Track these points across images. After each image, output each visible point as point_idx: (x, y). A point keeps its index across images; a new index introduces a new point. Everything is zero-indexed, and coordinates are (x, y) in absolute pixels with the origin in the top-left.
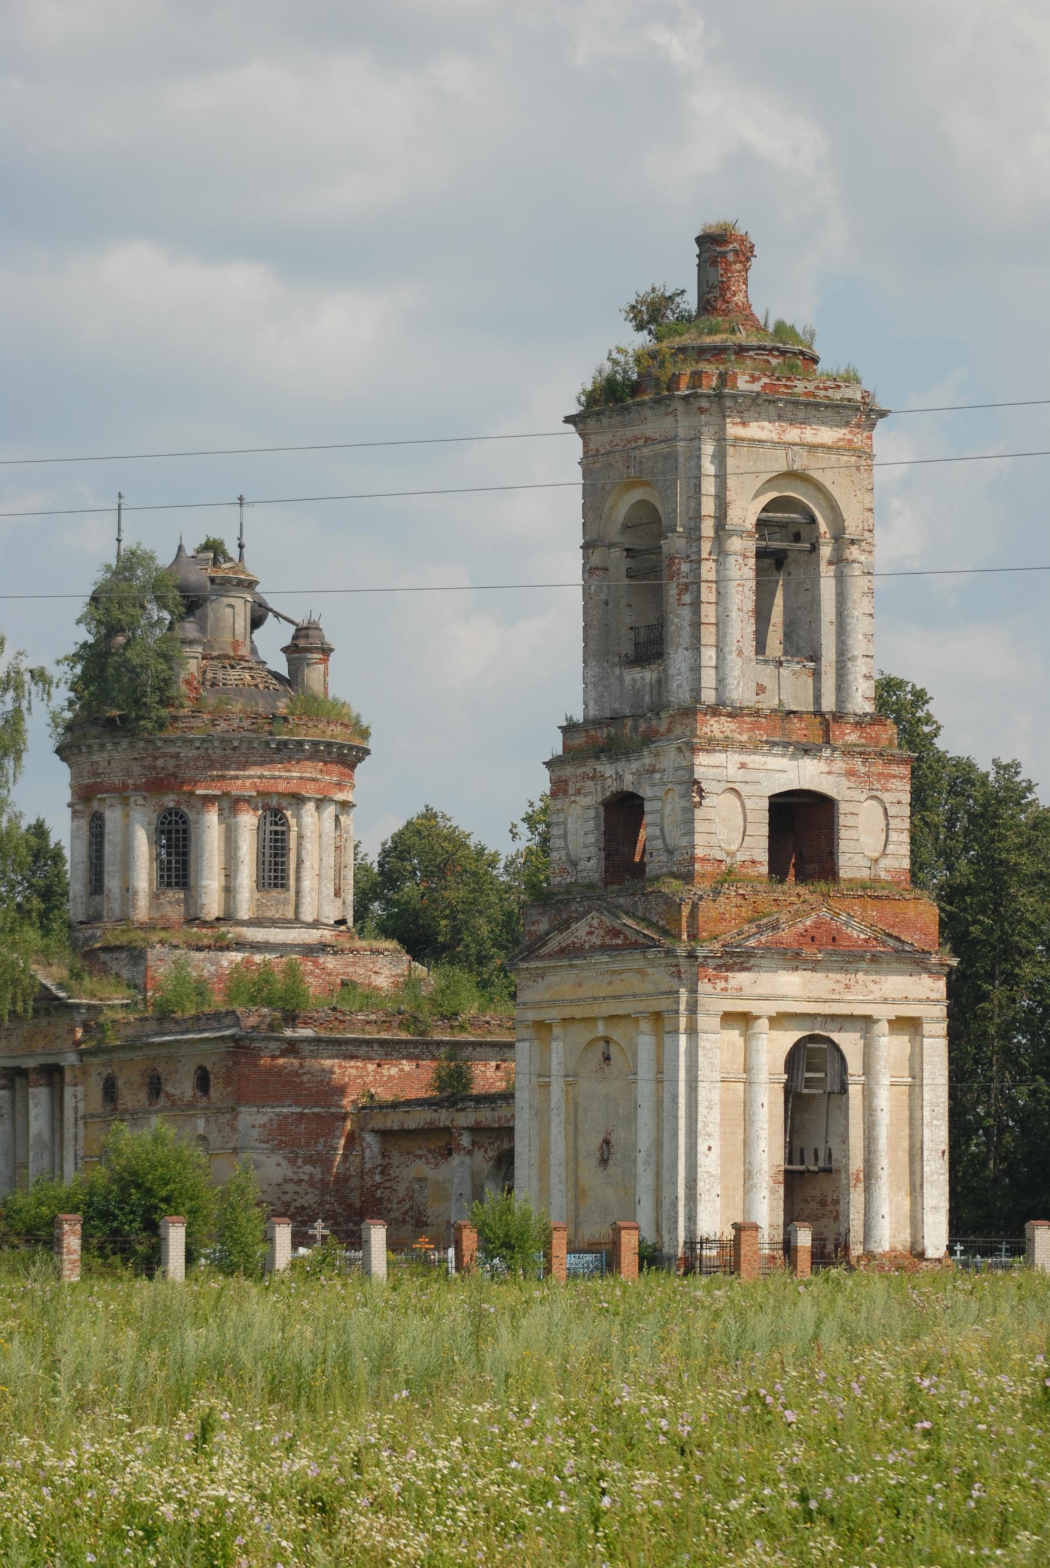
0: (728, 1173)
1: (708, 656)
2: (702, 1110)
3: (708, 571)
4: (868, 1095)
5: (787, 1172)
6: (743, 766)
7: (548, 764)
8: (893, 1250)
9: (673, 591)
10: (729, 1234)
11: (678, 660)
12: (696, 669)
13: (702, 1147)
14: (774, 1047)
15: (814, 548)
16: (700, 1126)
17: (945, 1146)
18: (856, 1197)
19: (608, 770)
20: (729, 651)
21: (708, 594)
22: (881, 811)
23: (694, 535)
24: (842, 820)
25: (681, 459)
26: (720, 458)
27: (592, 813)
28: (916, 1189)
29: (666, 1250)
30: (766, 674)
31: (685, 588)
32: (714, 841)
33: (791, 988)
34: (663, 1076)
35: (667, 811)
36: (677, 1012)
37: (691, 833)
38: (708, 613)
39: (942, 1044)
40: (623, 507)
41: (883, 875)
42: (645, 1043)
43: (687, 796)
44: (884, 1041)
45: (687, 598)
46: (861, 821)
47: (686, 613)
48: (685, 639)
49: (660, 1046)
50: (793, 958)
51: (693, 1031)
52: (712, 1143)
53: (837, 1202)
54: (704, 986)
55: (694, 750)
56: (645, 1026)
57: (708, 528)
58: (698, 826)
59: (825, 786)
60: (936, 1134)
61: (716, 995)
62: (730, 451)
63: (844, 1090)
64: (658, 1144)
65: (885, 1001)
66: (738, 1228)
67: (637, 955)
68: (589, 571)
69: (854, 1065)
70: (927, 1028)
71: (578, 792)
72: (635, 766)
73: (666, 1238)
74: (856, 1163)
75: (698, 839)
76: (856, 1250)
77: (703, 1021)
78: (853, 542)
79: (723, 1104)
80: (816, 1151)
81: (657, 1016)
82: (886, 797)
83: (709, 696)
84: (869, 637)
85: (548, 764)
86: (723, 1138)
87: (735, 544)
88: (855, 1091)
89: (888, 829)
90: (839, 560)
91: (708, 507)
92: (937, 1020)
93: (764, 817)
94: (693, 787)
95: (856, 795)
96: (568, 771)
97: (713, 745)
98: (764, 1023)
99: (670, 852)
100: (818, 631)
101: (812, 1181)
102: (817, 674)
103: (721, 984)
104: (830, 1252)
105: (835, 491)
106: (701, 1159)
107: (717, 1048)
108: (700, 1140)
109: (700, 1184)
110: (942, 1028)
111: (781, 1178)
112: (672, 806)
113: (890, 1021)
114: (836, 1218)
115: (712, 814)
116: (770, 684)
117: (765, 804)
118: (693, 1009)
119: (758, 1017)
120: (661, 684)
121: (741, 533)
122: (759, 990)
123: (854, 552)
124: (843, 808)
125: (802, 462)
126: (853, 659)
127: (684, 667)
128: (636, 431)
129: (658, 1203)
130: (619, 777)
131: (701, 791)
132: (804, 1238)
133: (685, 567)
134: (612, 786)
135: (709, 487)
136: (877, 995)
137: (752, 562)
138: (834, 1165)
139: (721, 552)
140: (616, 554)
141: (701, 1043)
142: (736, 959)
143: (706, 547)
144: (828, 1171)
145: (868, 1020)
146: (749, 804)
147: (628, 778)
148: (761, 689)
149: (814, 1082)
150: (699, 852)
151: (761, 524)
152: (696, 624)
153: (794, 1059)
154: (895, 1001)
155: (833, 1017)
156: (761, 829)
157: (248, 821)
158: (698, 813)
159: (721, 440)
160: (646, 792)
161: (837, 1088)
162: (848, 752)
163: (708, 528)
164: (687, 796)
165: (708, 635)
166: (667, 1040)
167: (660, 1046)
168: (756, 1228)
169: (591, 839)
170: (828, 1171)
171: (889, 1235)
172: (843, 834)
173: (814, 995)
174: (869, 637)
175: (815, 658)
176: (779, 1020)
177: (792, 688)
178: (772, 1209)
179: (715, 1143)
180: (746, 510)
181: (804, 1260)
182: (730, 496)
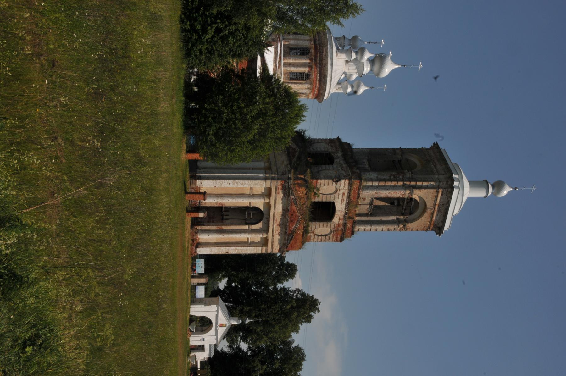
0: (218, 190)
1: (376, 184)
2: (242, 181)
3: (401, 183)
4: (245, 231)
5: (222, 207)
6: (343, 194)
7: (338, 138)
8: (199, 239)
9: (394, 173)
10: (202, 190)
11: (374, 175)
12: (372, 180)
13: (230, 181)
14: (259, 203)
15: (403, 214)
16: (237, 181)
17: (229, 253)
18: (214, 228)
19: (340, 154)
20: (373, 192)
21: (394, 183)
22: (327, 233)
23: (410, 180)
24: (325, 223)
25: (432, 176)
26: (432, 187)
27: (326, 150)
28: (218, 244)
29: (198, 170)
30: (368, 201)
31: (395, 177)
32: (322, 185)
33: (278, 209)
34: (253, 169)
35: (330, 171)
36: (272, 174)
37: (325, 178)
38: (388, 183)
39: (260, 252)
40: (414, 159)
41: (309, 235)
42: (262, 165)
43: (335, 177)
44: (261, 236)
45: (392, 177)
46: (325, 228)
47: (388, 177)
48: (380, 177)
49: (261, 169)
50: (286, 210)
51: (265, 179)
52: (231, 185)
53: (213, 222)
54: (280, 182)
55: (350, 179)
56: (267, 164)
57: (413, 183)
58: (327, 181)
59: (336, 220)
60: (233, 250)
61: (276, 186)
62: (435, 190)
63: (246, 224)
64: (231, 168)
65: (273, 236)
66: (205, 193)
67: (288, 162)
68: (394, 150)
69: (254, 227)
70: (264, 248)
71: (332, 146)
72: (342, 162)
73: (202, 170)
74: (225, 228)
75: (323, 181)
76: (198, 228)
77: (268, 182)
78: (404, 226)
79: (243, 188)
80: (228, 215)
81: (270, 168)
82: (331, 236)
83: (364, 183)
84: (376, 230)
85: (338, 138)
86: (233, 188)
87: (408, 192)
88: (246, 227)
89: (322, 236)
90: (398, 222)
91: (419, 183)
92: (266, 250)
93: (328, 200)
94: (338, 179)
95: (333, 226)
96: (338, 144)
97: (350, 185)
98: (267, 201)
99: (318, 172)
100: (379, 216)
101: (219, 216)
102: (366, 215)
103: (280, 187)
104: (196, 222)
105: (419, 220)
106: (226, 181)
107: (259, 186)
108: (232, 181)
109: (219, 181)
110: (264, 252)
111: (221, 206)
112: (333, 173)
113: (267, 237)
114: (208, 222)
115: (330, 185)
116: (365, 202)
117: (332, 201)
118: (273, 179)
119: (269, 199)
120: (366, 170)
121: (411, 193)
122: (278, 199)
123: (401, 226)
124: (329, 224)
125: (429, 211)
126: (371, 226)
127: (372, 177)
128: (437, 163)
129: (212, 168)
130: (338, 158)
131: (337, 181)
132: (201, 215)
133: (401, 177)
134: (335, 156)
135: (425, 183)
136: (275, 233)
137: (402, 196)
138: (224, 221)
139: (405, 187)
140: (400, 157)
141: (262, 181)
142: (287, 192)
143: (408, 183)
144: (222, 219)
145: (267, 231)
146: (332, 196)
147: (338, 160)
148: (364, 199)
149: (252, 216)
150: (319, 181)
151: (412, 199)
152: (385, 180)
153: (256, 209)
154: (273, 239)
155: (269, 221)
156: (324, 199)
157: (306, 70)
158: (331, 181)
159: (438, 188)
160: (335, 166)
161: (247, 222)
162: (345, 224)
163: (413, 183)
164: (335, 177)
165: (382, 184)
166: (263, 171)
167: (261, 169)
168: (205, 200)
169: (319, 150)
170: (222, 219)
171: (203, 238)
172: (322, 224)
173: (275, 215)
174: (376, 230)
175: (372, 215)
176: (268, 205)
177: (363, 208)
178: (211, 203)
179: (231, 186)
180: (417, 195)
181: (194, 215)
182: (422, 190)
